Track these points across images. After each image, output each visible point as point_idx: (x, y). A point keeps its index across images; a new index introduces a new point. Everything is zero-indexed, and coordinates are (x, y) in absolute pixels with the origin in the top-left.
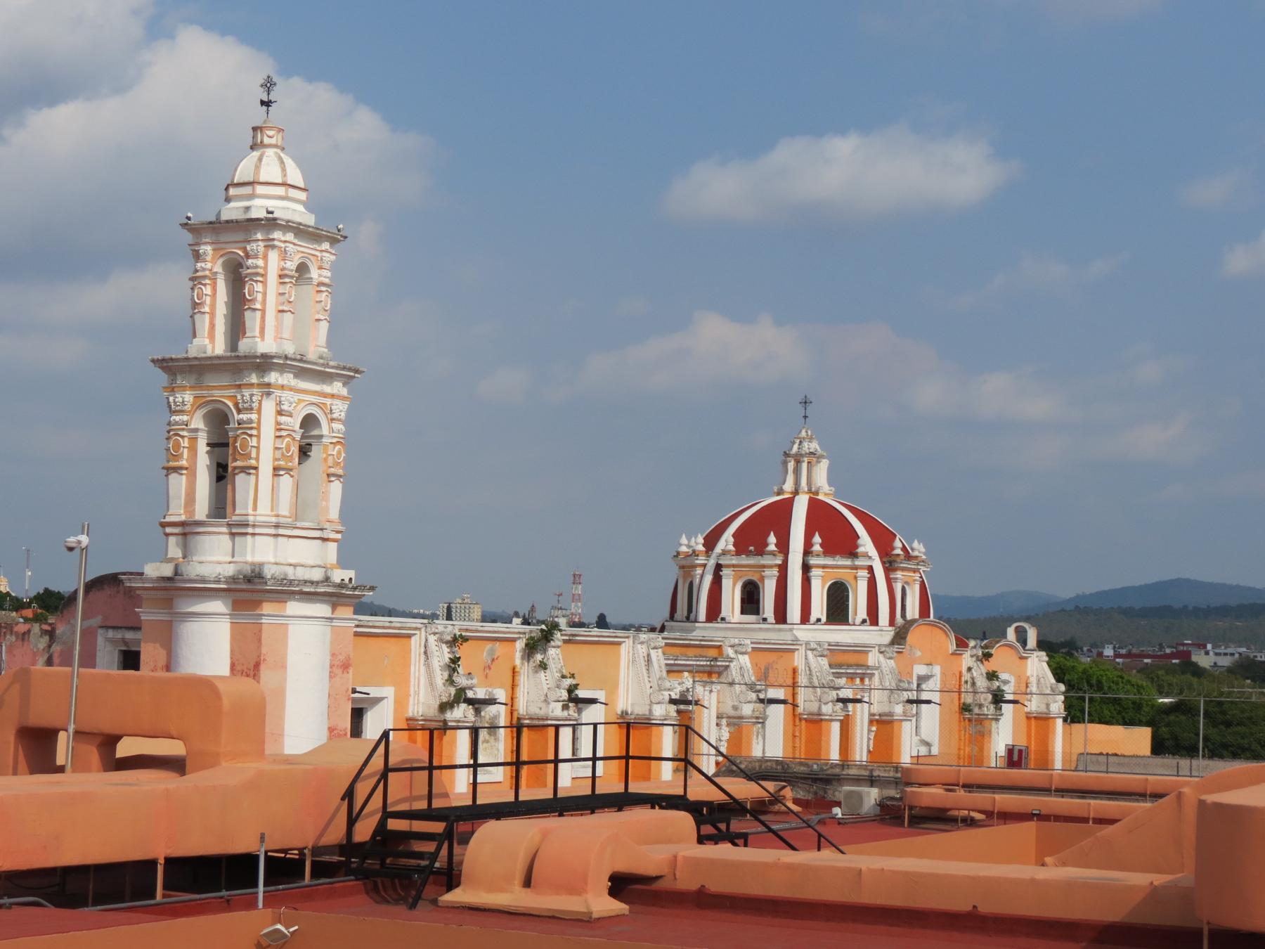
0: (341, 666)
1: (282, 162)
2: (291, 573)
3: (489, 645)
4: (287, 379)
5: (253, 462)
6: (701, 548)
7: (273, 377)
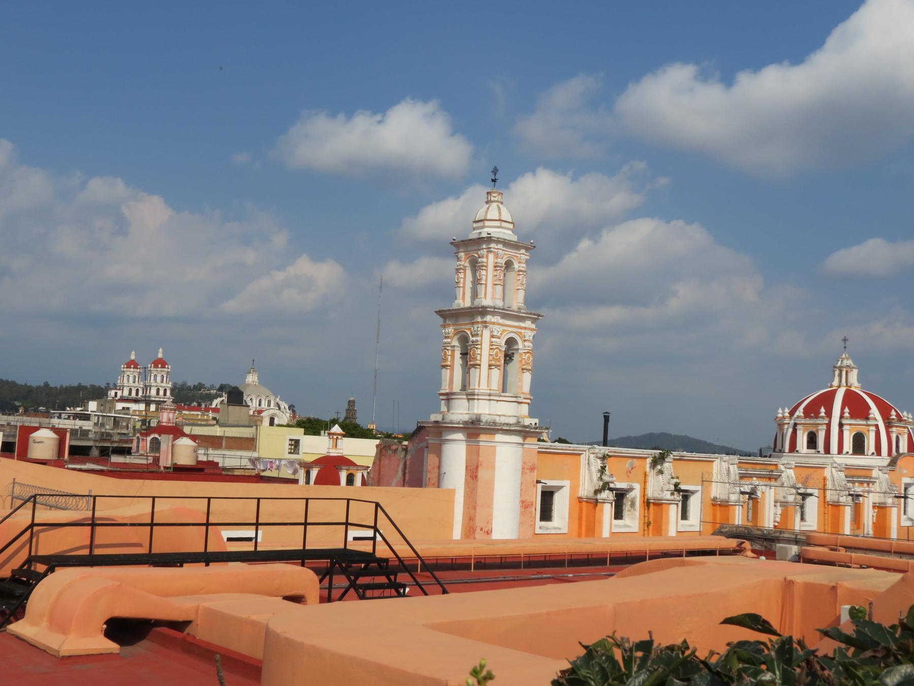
0: (528, 468)
1: (499, 209)
2: (498, 419)
3: (630, 460)
4: (497, 319)
5: (478, 362)
6: (787, 414)
7: (488, 318)
